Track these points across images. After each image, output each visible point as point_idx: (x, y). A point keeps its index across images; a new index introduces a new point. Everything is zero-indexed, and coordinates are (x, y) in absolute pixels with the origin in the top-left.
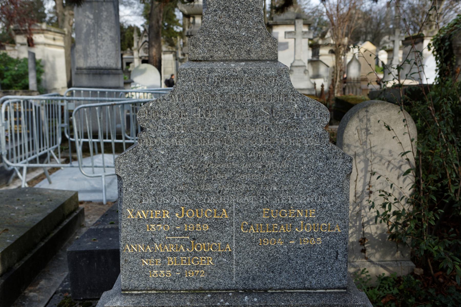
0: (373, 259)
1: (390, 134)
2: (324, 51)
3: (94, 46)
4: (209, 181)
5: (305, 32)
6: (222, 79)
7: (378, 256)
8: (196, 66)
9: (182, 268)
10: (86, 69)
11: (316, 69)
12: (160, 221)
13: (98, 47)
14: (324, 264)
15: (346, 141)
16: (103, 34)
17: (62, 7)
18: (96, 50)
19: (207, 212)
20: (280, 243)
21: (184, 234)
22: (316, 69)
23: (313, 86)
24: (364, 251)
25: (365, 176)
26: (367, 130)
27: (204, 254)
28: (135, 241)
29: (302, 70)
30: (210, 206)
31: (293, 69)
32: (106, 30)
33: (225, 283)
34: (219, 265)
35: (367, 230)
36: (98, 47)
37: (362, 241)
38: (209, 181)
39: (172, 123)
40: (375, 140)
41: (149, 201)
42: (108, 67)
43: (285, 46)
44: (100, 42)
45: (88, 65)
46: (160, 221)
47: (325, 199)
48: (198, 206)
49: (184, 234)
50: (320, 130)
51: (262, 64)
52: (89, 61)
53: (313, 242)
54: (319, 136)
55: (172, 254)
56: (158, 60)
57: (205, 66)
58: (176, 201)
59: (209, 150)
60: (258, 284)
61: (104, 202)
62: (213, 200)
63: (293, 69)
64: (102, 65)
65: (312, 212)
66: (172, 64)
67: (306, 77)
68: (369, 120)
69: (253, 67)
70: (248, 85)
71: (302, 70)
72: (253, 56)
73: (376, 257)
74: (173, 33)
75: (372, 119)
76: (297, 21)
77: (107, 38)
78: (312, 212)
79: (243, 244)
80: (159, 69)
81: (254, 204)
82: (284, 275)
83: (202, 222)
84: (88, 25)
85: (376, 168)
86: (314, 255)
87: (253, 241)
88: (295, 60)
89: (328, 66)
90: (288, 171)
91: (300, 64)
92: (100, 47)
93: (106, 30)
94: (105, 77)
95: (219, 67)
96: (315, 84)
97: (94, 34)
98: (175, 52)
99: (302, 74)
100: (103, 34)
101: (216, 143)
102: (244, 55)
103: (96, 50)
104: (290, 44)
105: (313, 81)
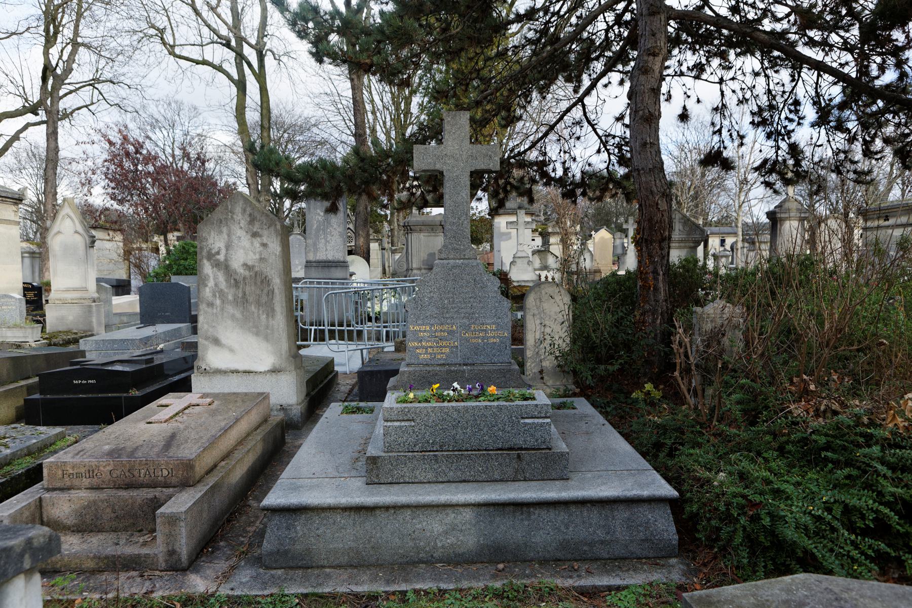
0: (548, 384)
1: (553, 301)
2: (553, 240)
3: (323, 241)
4: (447, 312)
5: (528, 222)
6: (453, 267)
7: (551, 382)
8: (441, 261)
9: (435, 354)
10: (315, 262)
11: (543, 260)
12: (425, 331)
13: (327, 241)
14: (501, 351)
15: (528, 306)
16: (333, 230)
17: (256, 192)
18: (326, 244)
19: (446, 327)
20: (480, 341)
21: (436, 337)
22: (543, 260)
23: (538, 278)
24: (542, 378)
25: (541, 329)
26: (540, 299)
27: (445, 347)
28: (413, 341)
29: (526, 260)
30: (448, 324)
31: (516, 260)
32: (335, 226)
33: (455, 361)
34: (452, 352)
35: (544, 364)
36: (327, 241)
37: (541, 372)
38: (447, 312)
39: (431, 286)
40: (545, 305)
41: (420, 322)
42: (336, 260)
43: (508, 236)
44: (329, 237)
45: (317, 258)
46: (425, 331)
47: (500, 320)
48: (442, 324)
49: (436, 337)
50: (496, 289)
51: (470, 261)
52: (318, 254)
53: (495, 341)
54: (495, 292)
55: (431, 347)
56: (365, 250)
57: (446, 262)
58: (432, 321)
59: (448, 298)
60: (470, 361)
61: (348, 373)
62: (449, 321)
63: (516, 260)
64: (330, 258)
65: (494, 327)
66: (377, 255)
67: (530, 268)
68: (541, 293)
69: (466, 261)
70: (464, 269)
71: (526, 260)
72: (466, 257)
73: (550, 383)
74: (376, 216)
75: (543, 292)
76: (518, 211)
77: (336, 233)
78: (494, 327)
79: (463, 342)
80: (368, 260)
81: (468, 323)
82: (482, 357)
83: (444, 331)
84: (318, 221)
85: (547, 323)
86: (496, 347)
87: (467, 340)
88: (518, 251)
89: (557, 257)
90: (483, 308)
91: (524, 255)
92: (329, 242)
93: (335, 226)
94: (333, 270)
95: (451, 261)
96: (540, 276)
97: (323, 230)
98: (381, 240)
99: (526, 265)
100: (333, 230)
101: (451, 295)
102: (462, 257)
103: (326, 244)
104: (512, 234)
105: (537, 272)
